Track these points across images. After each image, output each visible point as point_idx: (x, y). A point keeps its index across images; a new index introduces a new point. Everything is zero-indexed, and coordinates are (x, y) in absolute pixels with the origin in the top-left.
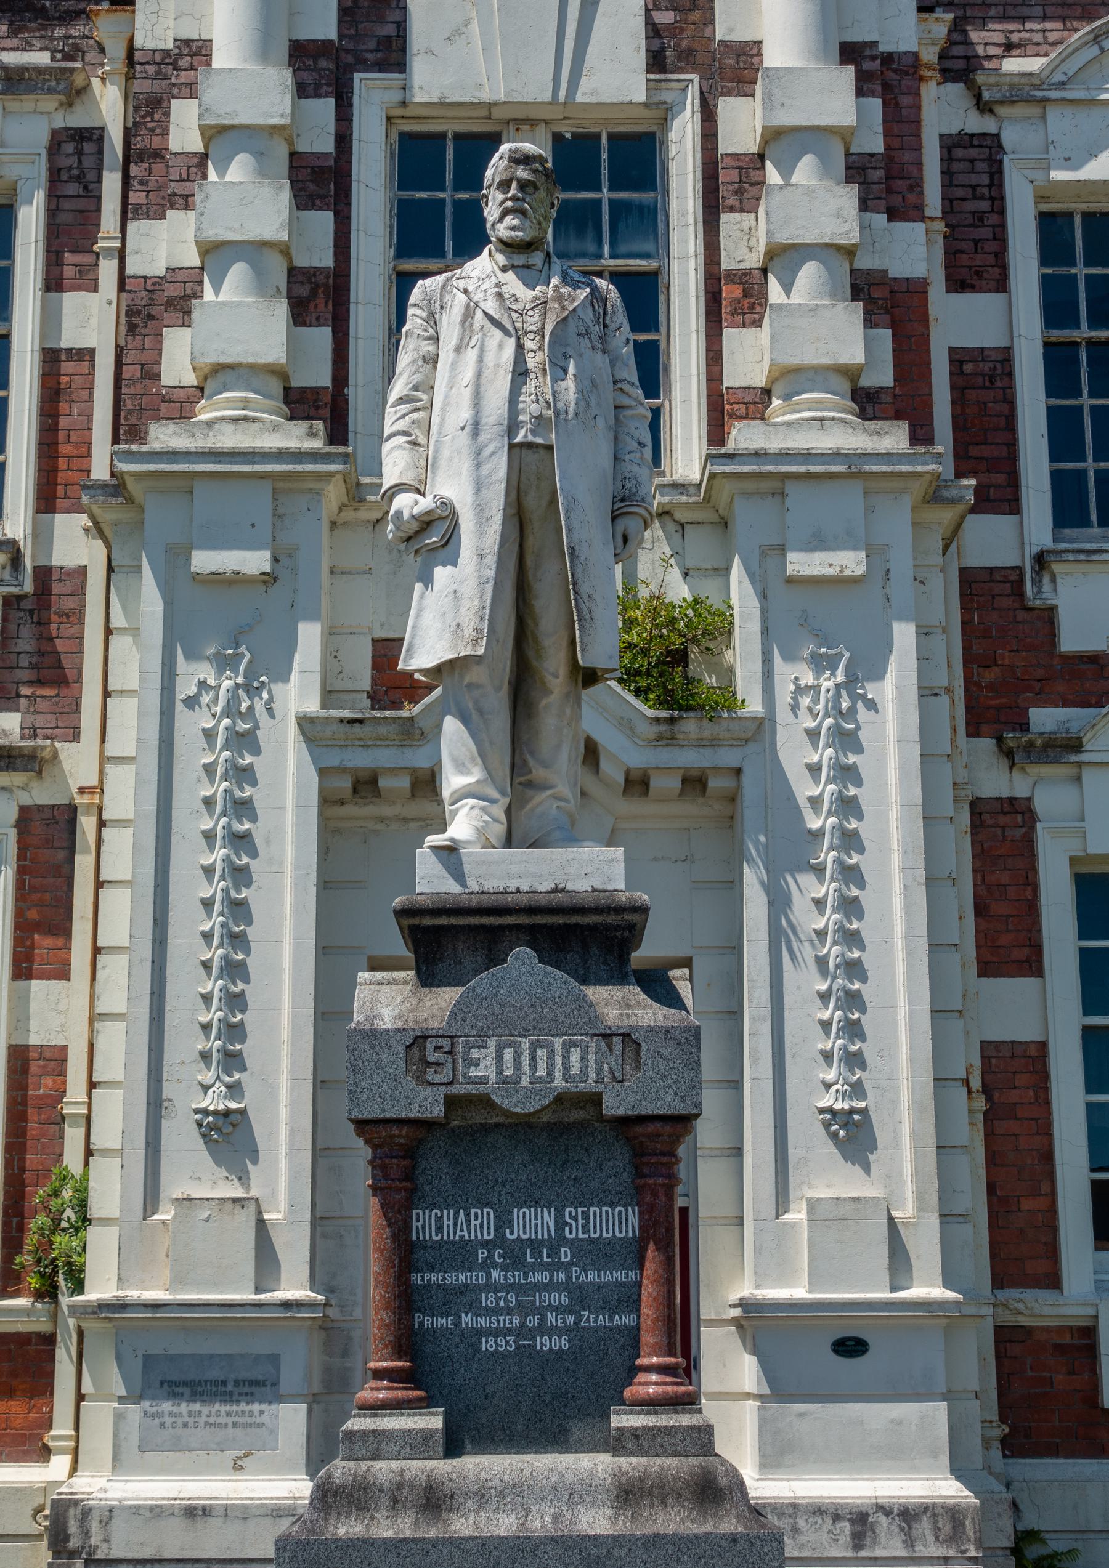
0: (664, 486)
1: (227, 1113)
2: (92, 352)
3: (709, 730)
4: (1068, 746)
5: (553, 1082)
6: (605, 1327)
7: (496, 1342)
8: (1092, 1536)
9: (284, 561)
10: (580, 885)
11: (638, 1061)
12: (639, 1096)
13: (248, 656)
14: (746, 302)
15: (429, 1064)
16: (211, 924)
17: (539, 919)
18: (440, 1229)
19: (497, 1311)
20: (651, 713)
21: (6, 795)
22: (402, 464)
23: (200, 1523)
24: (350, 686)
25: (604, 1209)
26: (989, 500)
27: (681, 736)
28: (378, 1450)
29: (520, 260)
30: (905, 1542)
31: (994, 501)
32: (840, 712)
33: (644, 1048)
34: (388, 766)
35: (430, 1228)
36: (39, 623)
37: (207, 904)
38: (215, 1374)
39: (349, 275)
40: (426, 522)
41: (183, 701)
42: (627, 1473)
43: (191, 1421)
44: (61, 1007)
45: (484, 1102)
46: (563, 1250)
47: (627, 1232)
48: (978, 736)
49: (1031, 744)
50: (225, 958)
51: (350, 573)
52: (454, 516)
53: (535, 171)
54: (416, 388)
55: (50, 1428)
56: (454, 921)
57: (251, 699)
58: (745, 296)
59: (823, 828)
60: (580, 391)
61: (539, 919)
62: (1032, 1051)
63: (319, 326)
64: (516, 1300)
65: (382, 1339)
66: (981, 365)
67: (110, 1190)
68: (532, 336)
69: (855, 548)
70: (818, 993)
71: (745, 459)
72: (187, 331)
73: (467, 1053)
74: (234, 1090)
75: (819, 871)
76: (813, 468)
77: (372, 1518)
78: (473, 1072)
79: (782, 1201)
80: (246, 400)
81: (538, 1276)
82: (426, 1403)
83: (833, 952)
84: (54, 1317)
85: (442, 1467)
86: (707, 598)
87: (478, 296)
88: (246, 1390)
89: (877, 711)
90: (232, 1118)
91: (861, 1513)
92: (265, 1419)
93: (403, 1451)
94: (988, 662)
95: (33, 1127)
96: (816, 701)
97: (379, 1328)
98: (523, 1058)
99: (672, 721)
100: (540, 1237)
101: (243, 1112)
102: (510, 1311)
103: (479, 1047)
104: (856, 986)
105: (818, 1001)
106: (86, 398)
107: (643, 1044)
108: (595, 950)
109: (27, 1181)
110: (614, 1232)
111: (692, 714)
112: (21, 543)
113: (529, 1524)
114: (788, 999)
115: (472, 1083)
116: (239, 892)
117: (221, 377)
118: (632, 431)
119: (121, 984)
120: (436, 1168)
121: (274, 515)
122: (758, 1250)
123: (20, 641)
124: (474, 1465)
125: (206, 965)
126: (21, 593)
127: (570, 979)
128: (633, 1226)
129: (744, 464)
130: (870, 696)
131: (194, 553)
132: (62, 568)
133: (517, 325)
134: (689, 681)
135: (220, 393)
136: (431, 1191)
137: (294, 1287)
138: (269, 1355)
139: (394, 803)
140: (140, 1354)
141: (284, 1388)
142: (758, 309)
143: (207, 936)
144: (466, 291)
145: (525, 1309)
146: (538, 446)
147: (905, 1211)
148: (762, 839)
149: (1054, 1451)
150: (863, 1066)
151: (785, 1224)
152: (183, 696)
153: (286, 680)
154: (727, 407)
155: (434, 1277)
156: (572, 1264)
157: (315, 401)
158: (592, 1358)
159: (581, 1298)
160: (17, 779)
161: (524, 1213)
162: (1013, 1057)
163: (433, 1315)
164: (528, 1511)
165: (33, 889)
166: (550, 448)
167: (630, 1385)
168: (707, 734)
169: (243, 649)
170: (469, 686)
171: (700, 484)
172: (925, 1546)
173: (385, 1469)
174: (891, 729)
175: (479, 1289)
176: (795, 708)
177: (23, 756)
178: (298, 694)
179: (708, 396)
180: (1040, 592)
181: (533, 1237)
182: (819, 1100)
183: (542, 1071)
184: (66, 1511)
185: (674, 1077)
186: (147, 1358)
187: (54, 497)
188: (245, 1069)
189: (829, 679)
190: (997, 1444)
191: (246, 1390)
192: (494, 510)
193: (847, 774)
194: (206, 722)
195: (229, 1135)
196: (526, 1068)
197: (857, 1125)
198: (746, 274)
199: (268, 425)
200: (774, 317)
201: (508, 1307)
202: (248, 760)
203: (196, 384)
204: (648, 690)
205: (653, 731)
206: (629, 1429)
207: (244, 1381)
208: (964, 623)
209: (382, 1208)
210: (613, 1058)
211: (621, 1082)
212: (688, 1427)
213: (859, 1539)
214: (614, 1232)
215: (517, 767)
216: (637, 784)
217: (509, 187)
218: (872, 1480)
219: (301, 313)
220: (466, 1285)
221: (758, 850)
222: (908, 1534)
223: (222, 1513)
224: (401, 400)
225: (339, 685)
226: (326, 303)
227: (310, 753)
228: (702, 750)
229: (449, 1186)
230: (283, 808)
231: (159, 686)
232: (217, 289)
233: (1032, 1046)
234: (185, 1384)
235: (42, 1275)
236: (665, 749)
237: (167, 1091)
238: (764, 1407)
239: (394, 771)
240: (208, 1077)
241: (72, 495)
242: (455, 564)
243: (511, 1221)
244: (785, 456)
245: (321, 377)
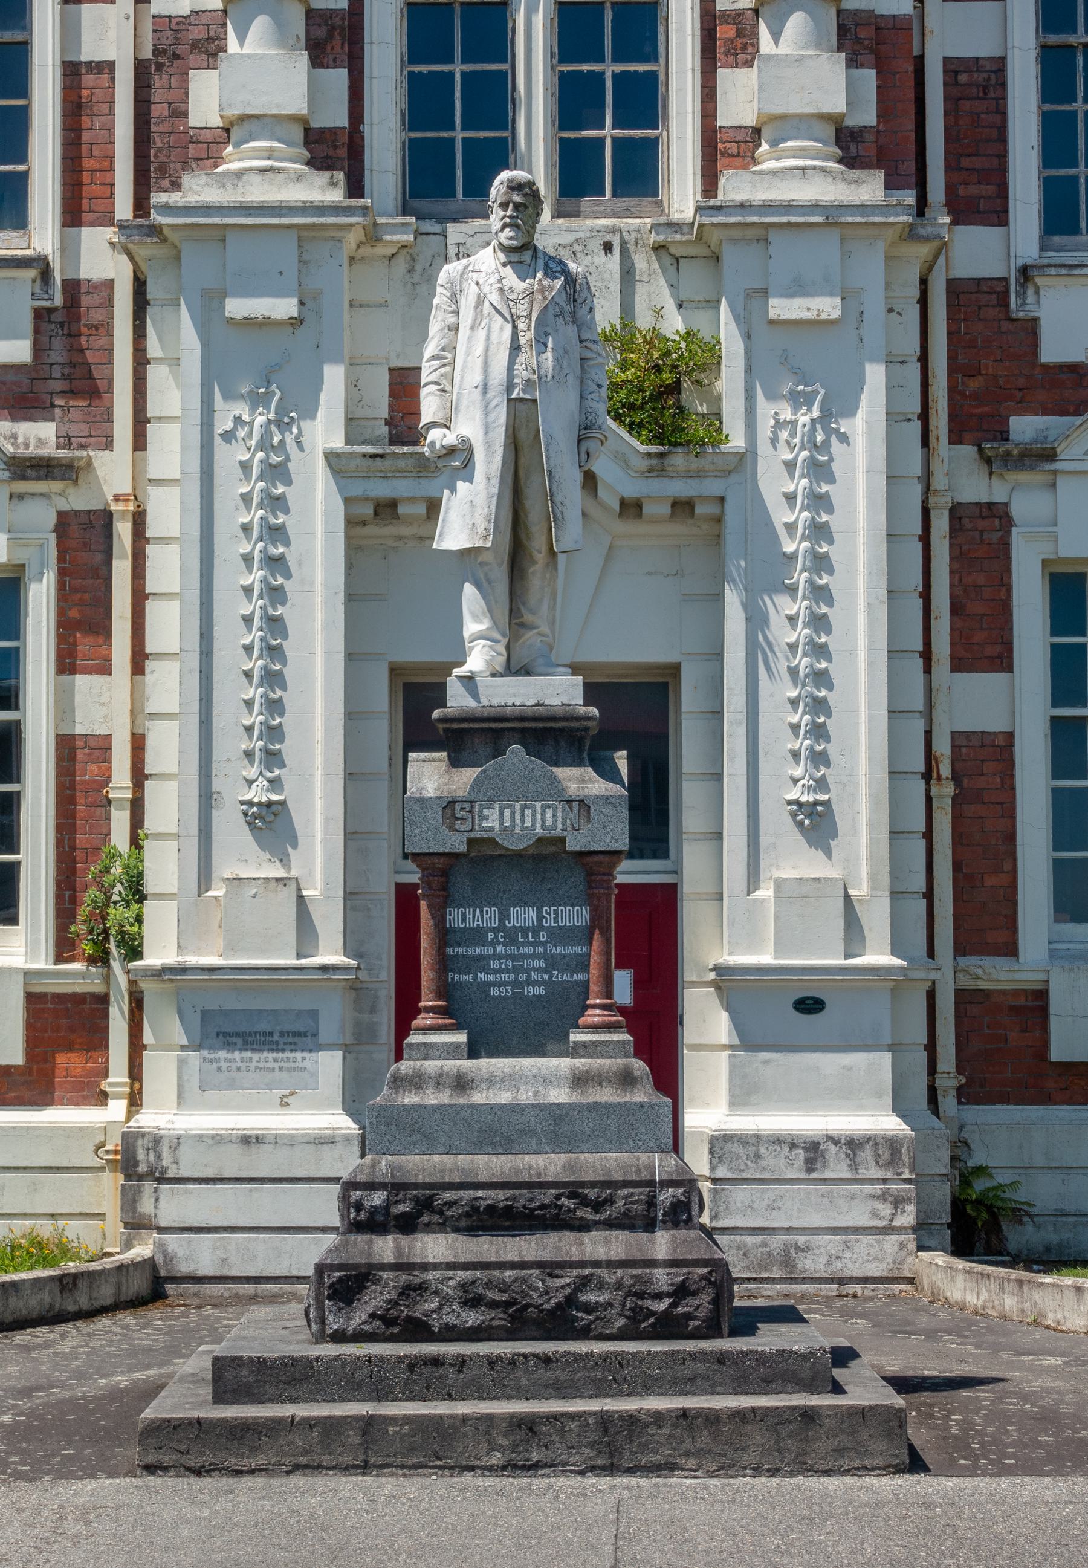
0: (660, 225)
1: (269, 804)
2: (111, 65)
3: (695, 464)
4: (1042, 455)
9: (309, 304)
10: (554, 701)
11: (588, 817)
12: (589, 839)
13: (278, 395)
14: (739, 43)
15: (457, 819)
16: (251, 638)
17: (526, 724)
18: (464, 920)
19: (500, 971)
20: (643, 449)
21: (45, 501)
22: (434, 407)
23: (254, 1148)
24: (369, 413)
26: (979, 212)
27: (670, 469)
29: (515, 257)
30: (850, 1166)
31: (984, 212)
32: (815, 445)
33: (592, 809)
34: (406, 495)
36: (69, 335)
37: (248, 620)
38: (263, 1026)
39: (363, 14)
40: (451, 451)
41: (220, 435)
43: (243, 1066)
44: (103, 699)
45: (492, 841)
48: (960, 443)
49: (1008, 453)
50: (265, 668)
51: (368, 306)
52: (471, 448)
53: (525, 195)
54: (443, 349)
55: (106, 1076)
56: (471, 725)
57: (282, 434)
58: (738, 36)
59: (797, 551)
60: (556, 359)
61: (526, 724)
62: (1000, 741)
63: (336, 67)
66: (976, 75)
67: (165, 868)
68: (523, 319)
69: (831, 294)
70: (789, 699)
71: (731, 210)
72: (214, 73)
73: (481, 812)
74: (275, 784)
75: (793, 590)
76: (794, 219)
77: (425, 1093)
78: (485, 824)
79: (753, 880)
80: (271, 149)
81: (526, 950)
82: (457, 1027)
83: (803, 663)
84: (107, 978)
85: (466, 1064)
86: (699, 331)
87: (486, 289)
88: (290, 1040)
89: (849, 444)
90: (274, 808)
91: (814, 1142)
92: (307, 1064)
94: (973, 372)
95: (81, 809)
96: (793, 435)
99: (662, 455)
101: (283, 803)
102: (508, 971)
104: (823, 693)
105: (789, 706)
106: (107, 111)
108: (563, 743)
109: (78, 859)
111: (679, 449)
112: (50, 258)
113: (519, 1097)
114: (763, 705)
116: (275, 609)
117: (247, 126)
118: (593, 376)
119: (168, 685)
120: (462, 883)
121: (300, 262)
122: (731, 924)
123: (52, 352)
124: (485, 1064)
125: (248, 674)
129: (730, 215)
130: (842, 430)
131: (227, 300)
132: (89, 281)
133: (513, 311)
134: (681, 410)
135: (246, 142)
137: (330, 953)
138: (309, 1011)
139: (411, 524)
141: (323, 1038)
142: (750, 49)
143: (248, 649)
144: (477, 284)
145: (516, 970)
146: (527, 400)
147: (860, 890)
148: (743, 563)
150: (827, 764)
151: (755, 900)
152: (220, 431)
153: (313, 417)
154: (719, 145)
155: (461, 950)
156: (547, 942)
157: (334, 141)
159: (553, 963)
160: (55, 486)
162: (982, 746)
164: (518, 1089)
165: (74, 590)
166: (536, 400)
168: (693, 466)
169: (274, 387)
170: (481, 564)
171: (693, 223)
172: (867, 1169)
173: (431, 1066)
174: (861, 461)
175: (489, 957)
176: (774, 441)
177: (61, 466)
178: (325, 431)
179: (703, 132)
180: (1024, 304)
182: (787, 793)
183: (528, 823)
184: (135, 1141)
186: (205, 1014)
188: (284, 766)
189: (805, 414)
190: (954, 1092)
191: (290, 1040)
192: (497, 447)
193: (819, 502)
194: (242, 454)
195: (271, 823)
196: (518, 821)
197: (820, 815)
198: (739, 15)
199: (292, 175)
200: (762, 67)
202: (281, 489)
203: (221, 125)
204: (641, 425)
205: (645, 464)
207: (288, 1033)
208: (950, 334)
213: (811, 1163)
215: (514, 612)
216: (631, 508)
217: (508, 207)
218: (825, 1116)
219: (319, 53)
220: (481, 955)
221: (739, 575)
222: (853, 1160)
223: (272, 1140)
224: (434, 358)
225: (360, 413)
226: (342, 45)
227: (337, 483)
228: (689, 481)
230: (313, 533)
231: (199, 422)
232: (242, 39)
233: (1001, 737)
234: (237, 1035)
236: (656, 480)
237: (216, 785)
238: (734, 1056)
239: (412, 500)
240: (252, 772)
241: (96, 209)
242: (471, 482)
243: (509, 915)
244: (768, 207)
245: (338, 117)
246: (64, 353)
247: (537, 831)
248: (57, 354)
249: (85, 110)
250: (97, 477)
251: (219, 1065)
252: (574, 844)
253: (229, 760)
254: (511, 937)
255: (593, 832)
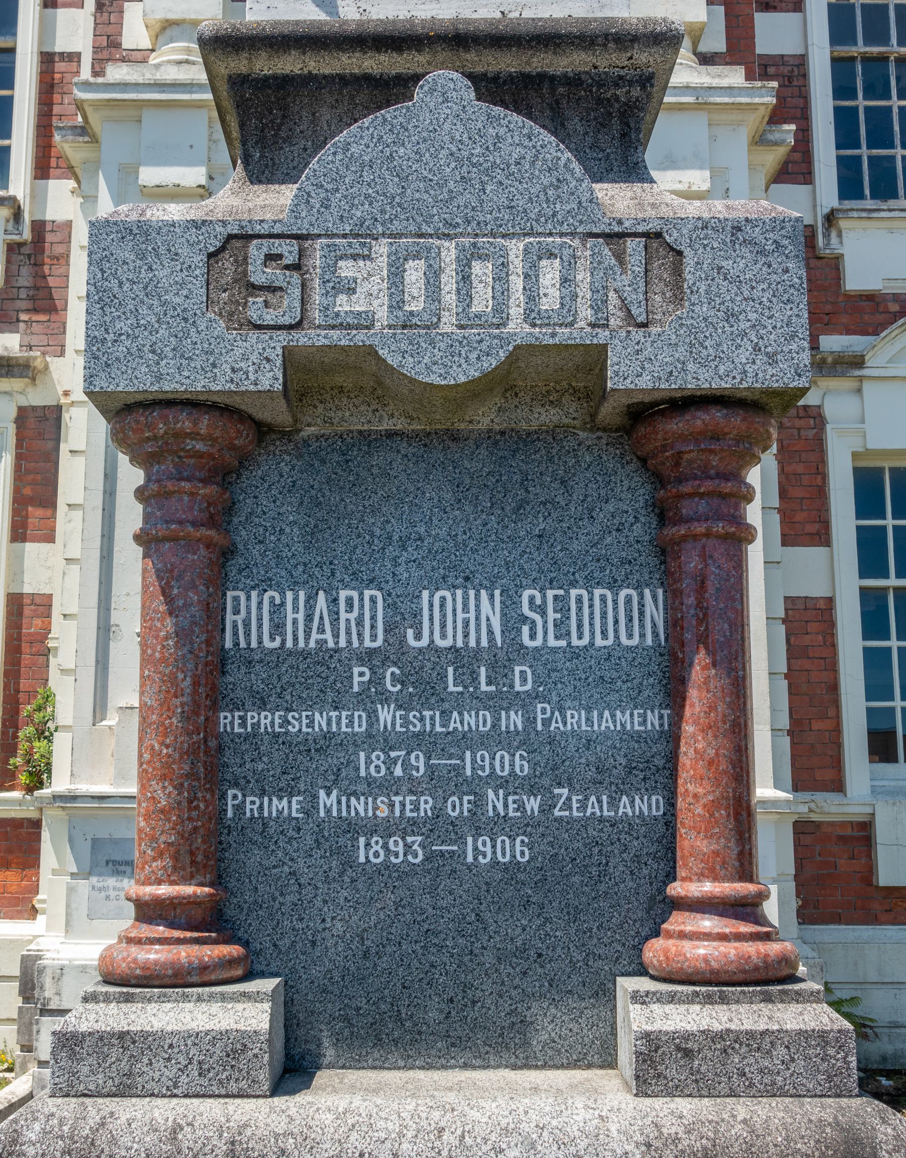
2: (79, 55)
5: (504, 325)
6: (602, 819)
7: (385, 846)
8: (867, 986)
12: (681, 352)
15: (254, 289)
18: (278, 628)
21: (7, 398)
25: (597, 592)
28: (129, 1075)
33: (689, 260)
35: (260, 626)
36: (35, 264)
42: (676, 1140)
46: (517, 669)
47: (642, 636)
64: (427, 764)
65: (154, 839)
78: (343, 304)
81: (470, 719)
93: (184, 1079)
95: (26, 658)
97: (147, 817)
98: (444, 278)
100: (472, 643)
103: (355, 257)
107: (687, 252)
110: (617, 637)
115: (341, 326)
120: (272, 502)
126: (21, 240)
127: (537, 129)
128: (654, 625)
136: (263, 555)
140: (89, 837)
145: (440, 782)
149: (836, 919)
155: (267, 720)
156: (536, 696)
158: (576, 879)
159: (554, 764)
160: (15, 384)
161: (443, 599)
162: (806, 609)
163: (263, 793)
165: (28, 471)
167: (656, 933)
175: (355, 742)
177: (19, 365)
180: (829, 244)
181: (460, 644)
183: (483, 301)
185: (753, 316)
187: (49, 167)
196: (450, 298)
201: (411, 778)
206: (673, 1036)
209: (159, 578)
210: (626, 279)
211: (644, 325)
212: (800, 1033)
214: (617, 637)
220: (328, 736)
229: (298, 548)
233: (821, 601)
235: (31, 773)
243: (417, 614)
246: (31, 279)
247: (511, 327)
248: (25, 280)
249: (56, 89)
250: (52, 379)
251: (108, 893)
252: (637, 369)
253: (128, 594)
254: (423, 682)
255: (693, 331)
